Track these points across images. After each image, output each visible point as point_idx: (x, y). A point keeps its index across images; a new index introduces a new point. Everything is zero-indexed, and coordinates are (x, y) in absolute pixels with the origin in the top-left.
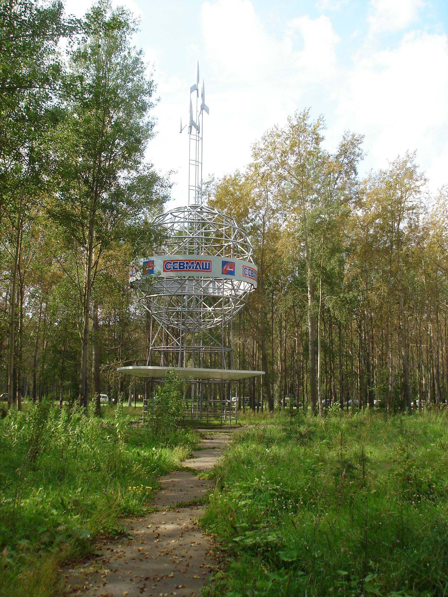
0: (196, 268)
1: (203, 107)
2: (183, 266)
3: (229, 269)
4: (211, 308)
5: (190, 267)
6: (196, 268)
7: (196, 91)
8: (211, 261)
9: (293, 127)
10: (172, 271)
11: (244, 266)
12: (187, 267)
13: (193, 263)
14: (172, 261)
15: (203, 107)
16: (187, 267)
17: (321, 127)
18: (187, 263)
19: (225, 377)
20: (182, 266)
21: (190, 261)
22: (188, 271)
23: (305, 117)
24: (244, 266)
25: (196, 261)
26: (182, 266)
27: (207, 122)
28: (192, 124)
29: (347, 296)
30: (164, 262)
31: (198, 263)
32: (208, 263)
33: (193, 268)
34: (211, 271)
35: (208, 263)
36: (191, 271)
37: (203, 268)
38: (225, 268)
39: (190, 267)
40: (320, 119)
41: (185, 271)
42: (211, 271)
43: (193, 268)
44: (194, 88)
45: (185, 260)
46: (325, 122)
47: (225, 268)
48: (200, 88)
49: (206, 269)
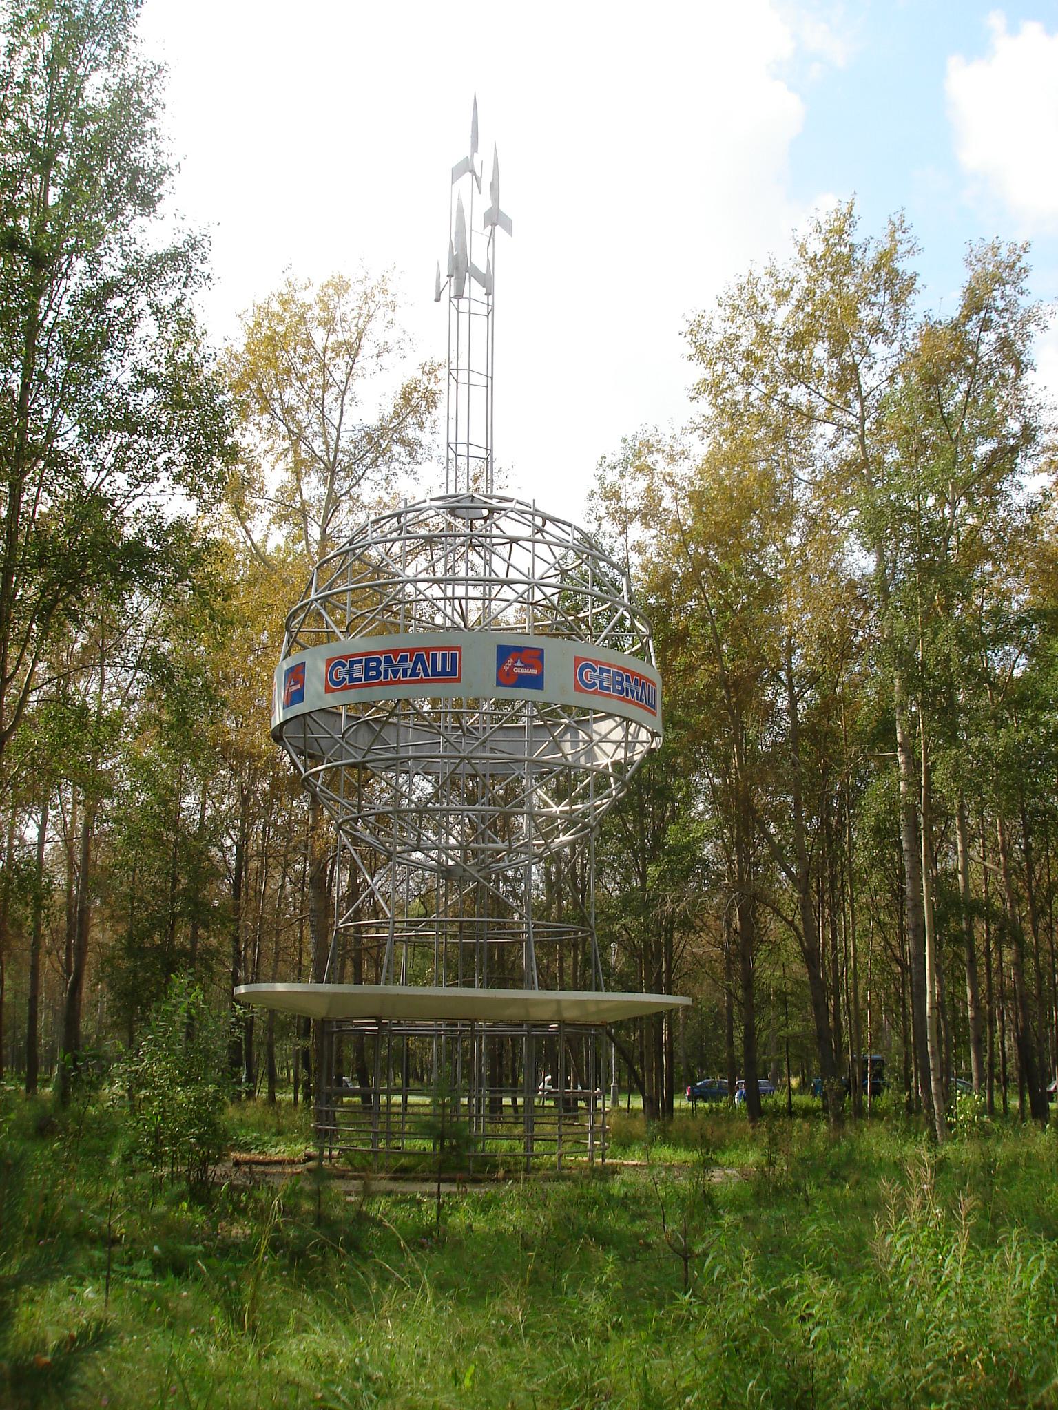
0: (414, 674)
1: (495, 218)
2: (376, 669)
3: (523, 671)
4: (561, 808)
5: (395, 672)
6: (414, 674)
7: (469, 175)
8: (459, 649)
9: (813, 261)
10: (346, 688)
11: (577, 660)
12: (386, 672)
13: (404, 659)
14: (346, 657)
15: (495, 218)
16: (386, 672)
17: (902, 248)
18: (388, 660)
19: (570, 1014)
20: (373, 669)
21: (395, 652)
22: (391, 683)
23: (843, 225)
24: (577, 660)
25: (412, 651)
26: (373, 669)
27: (507, 257)
28: (460, 268)
29: (990, 742)
30: (329, 662)
31: (420, 658)
32: (449, 654)
33: (405, 675)
34: (459, 680)
35: (449, 654)
36: (399, 682)
37: (434, 673)
38: (506, 668)
39: (395, 672)
40: (897, 227)
41: (381, 684)
42: (459, 680)
43: (405, 675)
44: (465, 167)
45: (381, 653)
46: (910, 233)
47: (506, 668)
48: (483, 161)
49: (444, 672)
